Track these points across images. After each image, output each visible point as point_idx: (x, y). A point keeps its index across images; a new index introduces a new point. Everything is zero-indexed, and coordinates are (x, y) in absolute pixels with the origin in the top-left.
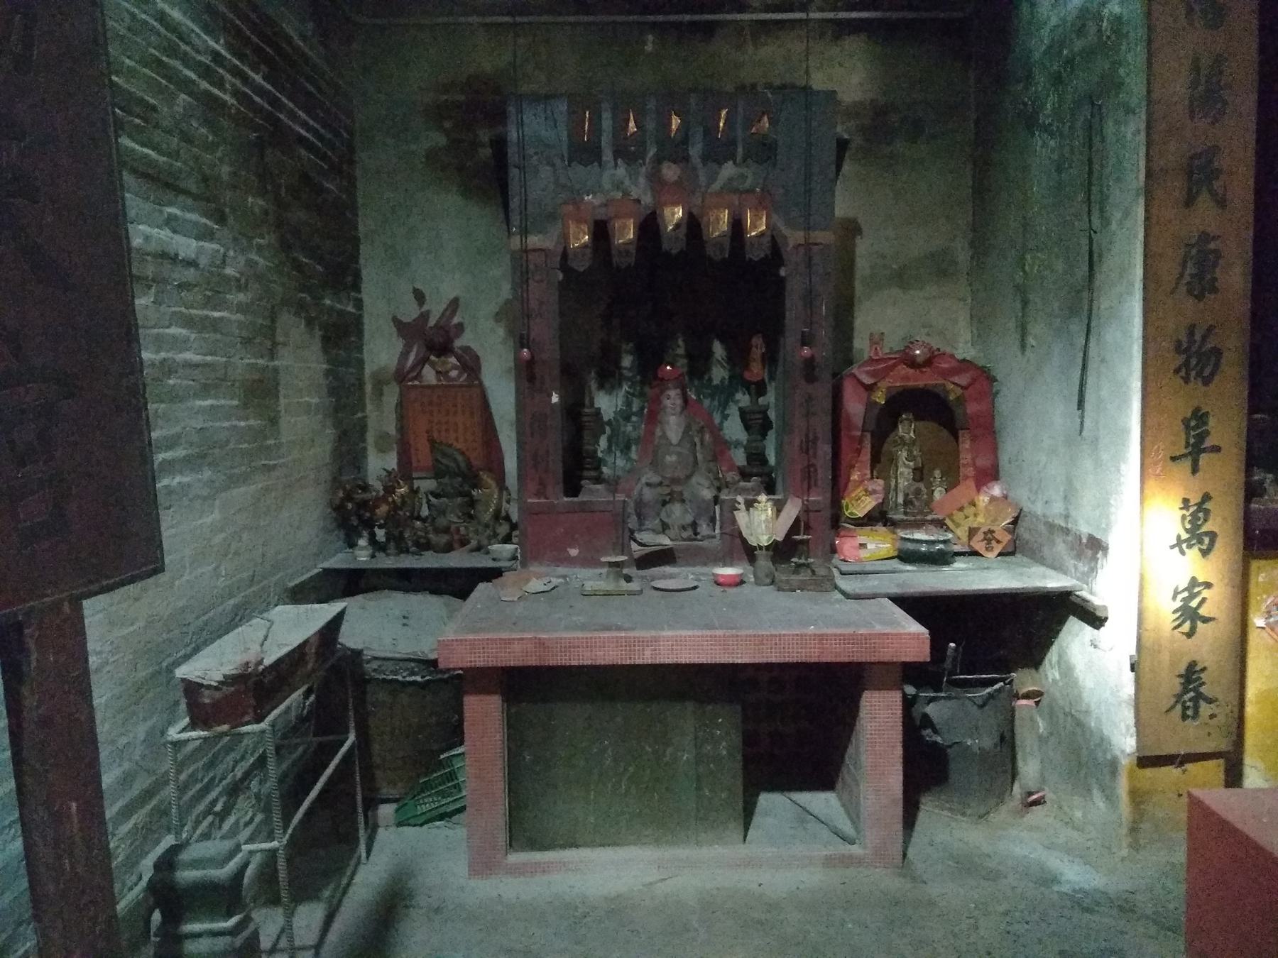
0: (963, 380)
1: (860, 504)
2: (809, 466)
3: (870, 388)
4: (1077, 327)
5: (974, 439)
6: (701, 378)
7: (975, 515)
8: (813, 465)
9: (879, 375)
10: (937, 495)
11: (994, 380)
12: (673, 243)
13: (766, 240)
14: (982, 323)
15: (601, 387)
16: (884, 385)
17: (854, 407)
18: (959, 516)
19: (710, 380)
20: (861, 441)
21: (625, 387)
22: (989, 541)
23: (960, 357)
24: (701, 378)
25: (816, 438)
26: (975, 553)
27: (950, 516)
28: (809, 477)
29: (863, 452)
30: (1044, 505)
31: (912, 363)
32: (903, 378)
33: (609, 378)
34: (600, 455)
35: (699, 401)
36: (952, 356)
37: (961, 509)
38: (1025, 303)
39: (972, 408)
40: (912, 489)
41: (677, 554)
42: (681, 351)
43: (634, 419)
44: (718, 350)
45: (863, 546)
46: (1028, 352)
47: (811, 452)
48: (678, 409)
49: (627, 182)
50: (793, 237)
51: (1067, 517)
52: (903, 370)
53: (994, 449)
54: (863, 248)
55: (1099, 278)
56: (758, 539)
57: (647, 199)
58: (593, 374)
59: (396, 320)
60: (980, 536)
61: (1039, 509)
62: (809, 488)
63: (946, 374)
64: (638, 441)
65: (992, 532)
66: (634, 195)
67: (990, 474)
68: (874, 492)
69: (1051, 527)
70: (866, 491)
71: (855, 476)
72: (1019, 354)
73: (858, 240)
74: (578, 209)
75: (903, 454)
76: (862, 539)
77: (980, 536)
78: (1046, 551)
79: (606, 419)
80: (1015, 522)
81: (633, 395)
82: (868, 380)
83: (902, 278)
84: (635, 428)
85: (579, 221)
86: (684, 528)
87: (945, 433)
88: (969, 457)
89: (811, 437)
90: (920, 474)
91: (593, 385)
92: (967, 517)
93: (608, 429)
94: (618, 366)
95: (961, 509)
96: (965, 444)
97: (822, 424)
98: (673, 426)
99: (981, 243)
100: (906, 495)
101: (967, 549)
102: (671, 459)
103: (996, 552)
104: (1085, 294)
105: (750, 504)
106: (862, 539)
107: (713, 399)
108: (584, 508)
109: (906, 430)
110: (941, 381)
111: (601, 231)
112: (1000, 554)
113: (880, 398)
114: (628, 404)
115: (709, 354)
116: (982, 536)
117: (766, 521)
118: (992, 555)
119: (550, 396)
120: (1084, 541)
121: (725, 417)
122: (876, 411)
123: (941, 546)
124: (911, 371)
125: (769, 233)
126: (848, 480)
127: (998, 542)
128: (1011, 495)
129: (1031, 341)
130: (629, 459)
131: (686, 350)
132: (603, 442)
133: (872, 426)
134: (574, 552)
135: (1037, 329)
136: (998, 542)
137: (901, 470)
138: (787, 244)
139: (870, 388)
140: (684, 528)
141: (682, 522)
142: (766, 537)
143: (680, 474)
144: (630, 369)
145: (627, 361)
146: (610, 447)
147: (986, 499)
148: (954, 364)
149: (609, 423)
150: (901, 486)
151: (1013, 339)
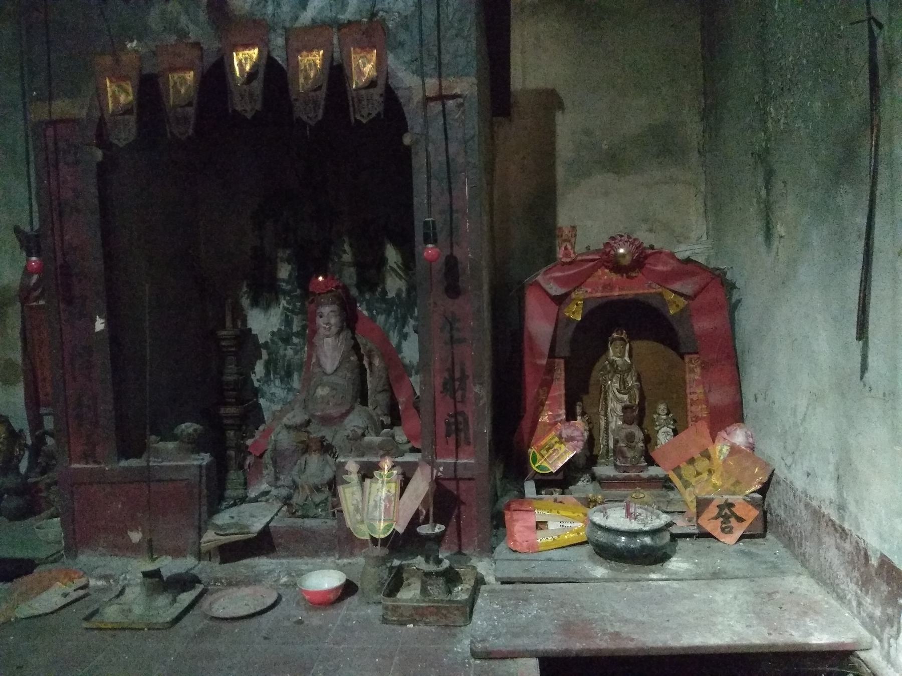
0: (687, 287)
1: (554, 454)
2: (456, 415)
3: (560, 300)
4: (850, 200)
5: (705, 366)
6: (372, 289)
7: (710, 472)
8: (463, 413)
9: (579, 281)
10: (664, 436)
11: (733, 286)
12: (246, 105)
13: (376, 93)
14: (716, 208)
15: (255, 303)
16: (579, 295)
17: (539, 326)
18: (688, 471)
19: (384, 292)
20: (550, 369)
21: (283, 303)
22: (726, 518)
23: (681, 256)
24: (372, 289)
25: (464, 377)
26: (707, 535)
27: (677, 470)
28: (457, 430)
29: (555, 384)
30: (809, 478)
31: (616, 266)
32: (605, 286)
33: (265, 292)
34: (256, 384)
35: (372, 318)
36: (672, 255)
37: (692, 461)
38: (769, 175)
39: (702, 325)
40: (623, 434)
41: (277, 541)
42: (347, 257)
43: (295, 340)
44: (392, 255)
45: (540, 525)
46: (775, 243)
47: (459, 394)
48: (334, 330)
49: (184, 19)
50: (407, 80)
51: (842, 508)
52: (605, 275)
53: (737, 382)
54: (566, 126)
55: (886, 112)
56: (372, 528)
57: (212, 45)
58: (245, 289)
59: (17, 230)
60: (713, 511)
61: (800, 483)
62: (457, 446)
63: (665, 279)
64: (300, 367)
65: (730, 505)
66: (193, 38)
67: (731, 414)
68: (570, 439)
69: (817, 515)
70: (560, 437)
71: (545, 418)
72: (763, 249)
73: (559, 117)
74: (117, 61)
75: (614, 385)
76: (540, 515)
77: (713, 511)
78: (808, 547)
79: (262, 341)
80: (764, 490)
81: (292, 311)
82: (556, 290)
83: (614, 161)
84: (296, 352)
85: (119, 78)
86: (317, 489)
87: (671, 354)
88: (700, 390)
89: (457, 375)
90: (638, 414)
91: (245, 302)
92: (698, 474)
93: (265, 355)
94: (274, 278)
95: (692, 461)
96: (694, 374)
97: (477, 355)
98: (330, 351)
99: (712, 112)
100: (616, 442)
101: (694, 530)
102: (321, 392)
103: (738, 534)
104: (867, 143)
105: (367, 472)
106: (540, 515)
107: (389, 315)
108: (146, 476)
109: (617, 354)
110: (656, 289)
111: (149, 88)
112: (742, 537)
113: (575, 313)
114: (288, 322)
115: (383, 261)
116: (716, 511)
117: (388, 498)
118: (730, 539)
119: (93, 321)
120: (874, 562)
121: (405, 336)
122: (569, 332)
123: (647, 540)
124: (614, 277)
125: (381, 82)
126: (535, 422)
127: (740, 520)
128: (760, 446)
129: (780, 229)
130: (290, 390)
131: (354, 255)
132: (259, 368)
133: (564, 350)
134: (136, 537)
135: (788, 209)
136: (740, 520)
137: (611, 405)
138: (410, 100)
139: (560, 300)
140: (317, 489)
141: (317, 481)
142: (382, 525)
143: (334, 412)
144: (287, 282)
145: (284, 272)
146: (268, 373)
147: (726, 449)
148: (673, 264)
149: (266, 346)
150: (612, 426)
151: (755, 225)
